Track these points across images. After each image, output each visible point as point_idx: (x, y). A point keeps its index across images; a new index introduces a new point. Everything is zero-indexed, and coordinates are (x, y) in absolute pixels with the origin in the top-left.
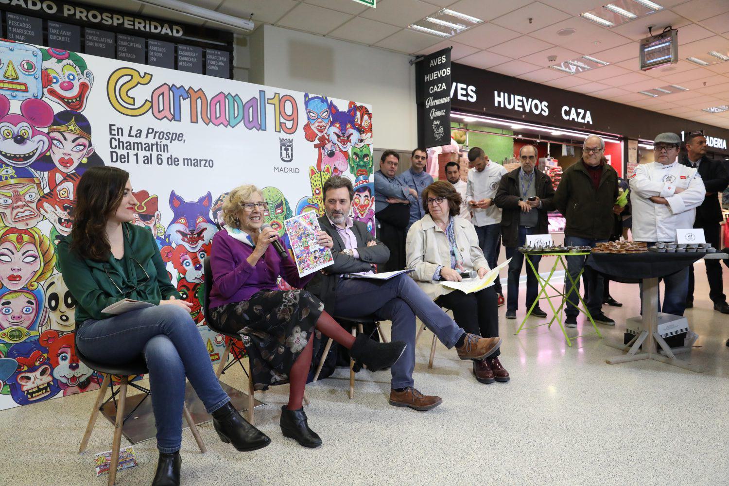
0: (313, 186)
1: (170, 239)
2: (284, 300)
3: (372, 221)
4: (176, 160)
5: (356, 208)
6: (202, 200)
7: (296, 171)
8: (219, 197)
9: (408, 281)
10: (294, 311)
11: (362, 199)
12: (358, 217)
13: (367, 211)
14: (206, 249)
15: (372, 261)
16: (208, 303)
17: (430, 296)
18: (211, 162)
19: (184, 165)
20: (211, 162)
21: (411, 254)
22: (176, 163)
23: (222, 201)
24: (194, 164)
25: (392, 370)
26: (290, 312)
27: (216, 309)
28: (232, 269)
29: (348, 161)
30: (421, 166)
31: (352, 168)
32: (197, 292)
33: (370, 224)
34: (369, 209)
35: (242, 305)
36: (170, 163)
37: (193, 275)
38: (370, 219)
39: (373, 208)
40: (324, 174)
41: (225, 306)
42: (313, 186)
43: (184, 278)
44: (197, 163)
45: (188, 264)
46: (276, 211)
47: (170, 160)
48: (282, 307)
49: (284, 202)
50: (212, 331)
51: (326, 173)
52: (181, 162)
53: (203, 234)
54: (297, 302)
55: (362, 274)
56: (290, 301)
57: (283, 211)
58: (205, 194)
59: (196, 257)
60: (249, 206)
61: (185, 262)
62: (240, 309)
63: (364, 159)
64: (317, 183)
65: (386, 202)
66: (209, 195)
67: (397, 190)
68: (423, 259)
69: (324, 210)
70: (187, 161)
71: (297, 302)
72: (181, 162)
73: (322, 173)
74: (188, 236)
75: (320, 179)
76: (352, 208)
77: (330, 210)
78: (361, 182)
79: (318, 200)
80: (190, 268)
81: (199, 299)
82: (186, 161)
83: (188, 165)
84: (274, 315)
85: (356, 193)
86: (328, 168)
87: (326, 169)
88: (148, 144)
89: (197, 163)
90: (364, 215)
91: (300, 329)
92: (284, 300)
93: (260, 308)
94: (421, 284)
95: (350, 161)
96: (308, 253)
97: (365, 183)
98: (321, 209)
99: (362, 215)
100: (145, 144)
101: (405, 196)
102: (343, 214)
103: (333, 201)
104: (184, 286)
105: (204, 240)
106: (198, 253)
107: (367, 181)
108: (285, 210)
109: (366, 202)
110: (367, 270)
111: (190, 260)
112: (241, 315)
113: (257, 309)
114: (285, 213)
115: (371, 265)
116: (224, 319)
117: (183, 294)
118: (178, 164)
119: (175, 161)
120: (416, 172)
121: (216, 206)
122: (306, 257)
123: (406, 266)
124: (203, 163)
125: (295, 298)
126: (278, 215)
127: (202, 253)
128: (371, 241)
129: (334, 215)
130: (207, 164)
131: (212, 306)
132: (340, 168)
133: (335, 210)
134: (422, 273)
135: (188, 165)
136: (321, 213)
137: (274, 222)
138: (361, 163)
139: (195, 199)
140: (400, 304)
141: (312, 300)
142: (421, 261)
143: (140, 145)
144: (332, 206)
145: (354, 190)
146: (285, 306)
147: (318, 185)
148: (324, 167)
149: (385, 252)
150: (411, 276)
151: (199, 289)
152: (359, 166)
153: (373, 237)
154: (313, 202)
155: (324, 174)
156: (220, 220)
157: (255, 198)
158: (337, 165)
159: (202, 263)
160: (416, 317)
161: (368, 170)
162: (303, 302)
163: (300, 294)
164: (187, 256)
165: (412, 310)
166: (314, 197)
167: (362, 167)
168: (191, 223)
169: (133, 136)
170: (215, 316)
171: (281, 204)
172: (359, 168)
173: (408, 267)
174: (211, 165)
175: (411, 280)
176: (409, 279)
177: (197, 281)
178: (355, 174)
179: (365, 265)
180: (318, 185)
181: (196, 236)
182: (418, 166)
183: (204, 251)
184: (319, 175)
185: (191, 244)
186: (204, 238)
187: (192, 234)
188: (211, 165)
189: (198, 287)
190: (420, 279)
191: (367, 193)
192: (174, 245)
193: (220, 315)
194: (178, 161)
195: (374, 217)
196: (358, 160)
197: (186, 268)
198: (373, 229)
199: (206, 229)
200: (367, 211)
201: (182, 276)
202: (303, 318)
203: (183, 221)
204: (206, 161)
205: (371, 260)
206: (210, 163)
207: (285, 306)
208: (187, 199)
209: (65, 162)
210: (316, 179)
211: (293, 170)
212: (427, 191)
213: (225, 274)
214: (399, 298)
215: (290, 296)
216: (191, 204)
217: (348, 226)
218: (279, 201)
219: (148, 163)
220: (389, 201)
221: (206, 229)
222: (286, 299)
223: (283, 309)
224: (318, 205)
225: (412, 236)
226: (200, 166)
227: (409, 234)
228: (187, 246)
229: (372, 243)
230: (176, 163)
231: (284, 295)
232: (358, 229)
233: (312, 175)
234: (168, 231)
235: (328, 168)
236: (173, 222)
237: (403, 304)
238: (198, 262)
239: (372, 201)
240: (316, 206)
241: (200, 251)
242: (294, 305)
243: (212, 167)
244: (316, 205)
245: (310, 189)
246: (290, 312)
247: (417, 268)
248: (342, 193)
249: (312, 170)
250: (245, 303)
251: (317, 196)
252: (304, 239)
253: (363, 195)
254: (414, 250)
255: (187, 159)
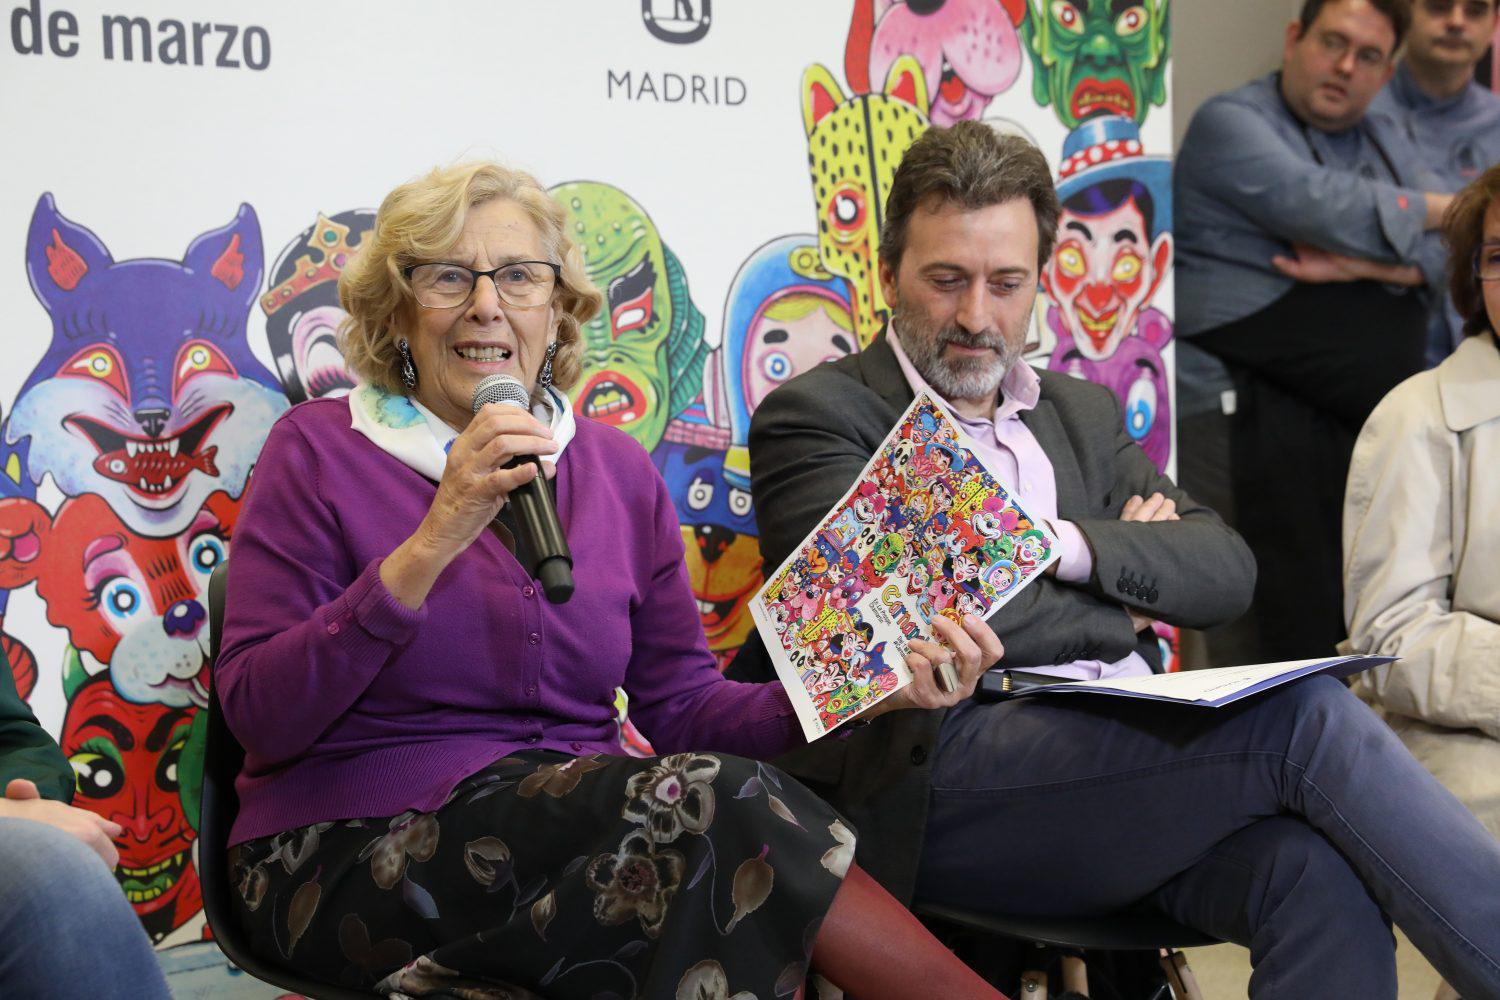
0: (825, 181)
1: (31, 461)
2: (630, 816)
3: (1157, 374)
4: (63, 24)
5: (1067, 302)
6: (205, 249)
7: (730, 92)
8: (305, 238)
9: (1343, 721)
10: (687, 875)
11: (1100, 248)
12: (1074, 353)
13: (1126, 322)
14: (217, 516)
15: (1157, 606)
16: (224, 808)
17: (1482, 818)
18: (256, 39)
19: (109, 53)
20: (256, 39)
21: (1373, 566)
22: (64, 42)
23: (317, 255)
24: (164, 46)
25: (45, 737)
26: (667, 880)
27: (262, 847)
28: (301, 616)
29: (1022, 32)
30: (1461, 55)
31: (1044, 72)
32: (173, 757)
33: (1142, 392)
34: (1138, 310)
35: (402, 837)
36: (27, 39)
37: (153, 661)
38: (1142, 363)
39: (1165, 300)
40: (887, 111)
41: (311, 836)
42: (825, 181)
43: (105, 676)
44: (180, 44)
45: (124, 601)
46: (614, 319)
47: (26, 23)
48: (622, 857)
49: (659, 268)
50: (245, 977)
51: (896, 102)
52: (90, 36)
53: (212, 439)
54: (702, 824)
55: (1081, 674)
56: (663, 822)
57: (653, 317)
58: (223, 217)
59: (174, 563)
60: (447, 277)
61: (111, 588)
62: (390, 856)
63: (1112, 18)
64: (847, 160)
65: (1277, 274)
66: (247, 225)
67: (1342, 204)
68: (1450, 595)
69: (881, 315)
70: (124, 33)
71: (702, 824)
72: (90, 36)
73: (875, 102)
74: (131, 449)
75: (860, 139)
76: (1043, 302)
77: (930, 322)
78: (1096, 154)
79: (848, 257)
80: (137, 624)
81: (185, 793)
82: (117, 29)
83: (128, 55)
84: (577, 899)
85: (1068, 217)
86: (907, 77)
87: (895, 80)
88: (179, 26)
89: (180, 44)
90: (1113, 343)
91: (723, 982)
92: (630, 816)
93: (498, 853)
94: (1432, 740)
95: (1032, 32)
96: (847, 593)
97: (1119, 161)
98: (864, 310)
99: (1099, 342)
100: (163, 26)
101: (1387, 245)
102: (997, 350)
103: (959, 278)
104: (103, 722)
105: (215, 473)
106: (181, 543)
107: (1132, 146)
108: (664, 310)
109: (1124, 271)
110: (1112, 653)
111: (137, 581)
112: (399, 885)
113: (486, 858)
114: (663, 330)
115: (1139, 623)
116: (305, 909)
117: (95, 766)
118: (74, 49)
119: (55, 33)
120: (1427, 88)
121: (286, 286)
122: (829, 586)
123: (1343, 634)
124: (213, 43)
125: (692, 803)
126: (624, 339)
127: (203, 540)
128: (1146, 497)
129: (953, 353)
130: (236, 52)
131: (241, 833)
132: (976, 74)
133: (964, 330)
134: (1442, 680)
135: (128, 55)
136: (863, 329)
137: (603, 376)
138: (1100, 44)
139: (172, 248)
140: (1292, 848)
141: (787, 815)
142: (1434, 607)
143: (137, 32)
144: (942, 306)
145: (1061, 198)
146: (638, 846)
147: (850, 173)
148: (883, 70)
149: (1225, 558)
150: (1371, 698)
151: (185, 737)
152: (1083, 60)
153: (1160, 475)
154: (820, 269)
155: (887, 111)
156: (314, 360)
157: (500, 235)
158: (959, 62)
159: (203, 599)
160: (1397, 931)
161: (1138, 84)
162: (739, 828)
163: (719, 784)
164: (124, 558)
165: (1371, 893)
166: (826, 240)
167: (1101, 69)
168: (146, 372)
169: (219, 28)
170: (254, 888)
171: (646, 277)
172: (1087, 73)
173: (1355, 642)
174: (257, 58)
175: (1372, 719)
176: (1353, 713)
177: (176, 697)
178: (1060, 111)
179: (1102, 624)
180: (850, 173)
181: (173, 448)
182: (1442, 53)
183: (215, 531)
184: (857, 116)
185: (146, 493)
186: (218, 461)
187: (154, 436)
188: (257, 58)
189: (180, 729)
190: (1425, 712)
191: (1128, 217)
192: (50, 497)
193: (284, 884)
194: (73, 30)
195: (1168, 355)
196: (1078, 27)
197: (117, 622)
198: (1160, 423)
199: (228, 409)
200: (1126, 322)
201: (93, 666)
202: (738, 917)
203: (100, 363)
204: (232, 31)
205: (1152, 596)
206: (251, 48)
207: (638, 846)
208: (125, 244)
209: (959, 577)
210: (843, 135)
211: (709, 91)
212: (1477, 199)
213: (267, 637)
214: (1291, 815)
215: (661, 792)
216: (149, 273)
217: (1011, 407)
218: (633, 266)
219: (182, 58)
220: (1293, 268)
221: (228, 409)
222: (638, 806)
223: (630, 867)
224: (847, 282)
225: (1379, 462)
226: (199, 60)
227: (1364, 449)
228: (121, 499)
229: (1157, 509)
230: (64, 42)
231: (632, 782)
232: (1067, 419)
233: (818, 115)
234: (16, 415)
235: (907, 77)
236: (50, 367)
237: (1318, 858)
238: (183, 590)
239: (1158, 263)
240: (838, 293)
241: (195, 530)
242: (687, 843)
243: (264, 65)
244: (838, 286)
245: (806, 194)
246: (667, 880)
247: (1409, 648)
248: (1001, 230)
249: (817, 87)
250: (423, 824)
251: (844, 236)
252: (899, 540)
253: (1104, 227)
254: (1393, 543)
255: (122, 20)
